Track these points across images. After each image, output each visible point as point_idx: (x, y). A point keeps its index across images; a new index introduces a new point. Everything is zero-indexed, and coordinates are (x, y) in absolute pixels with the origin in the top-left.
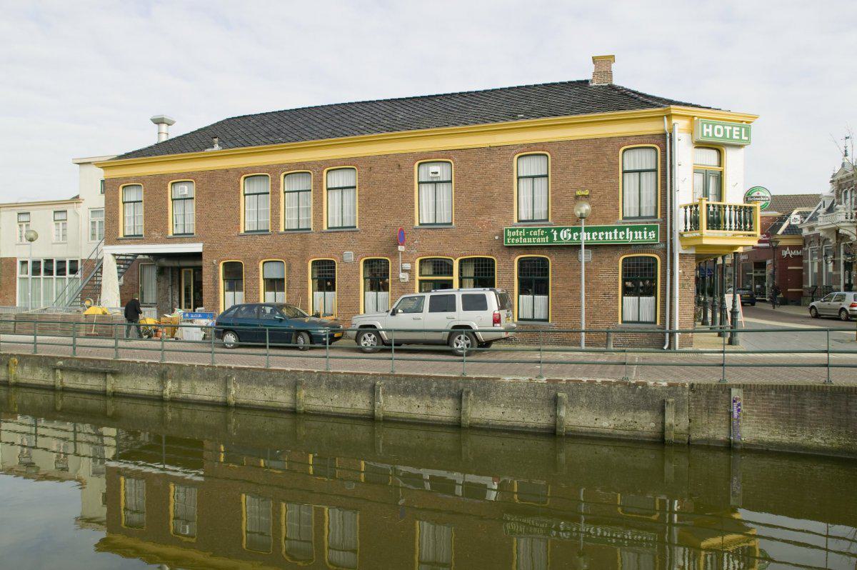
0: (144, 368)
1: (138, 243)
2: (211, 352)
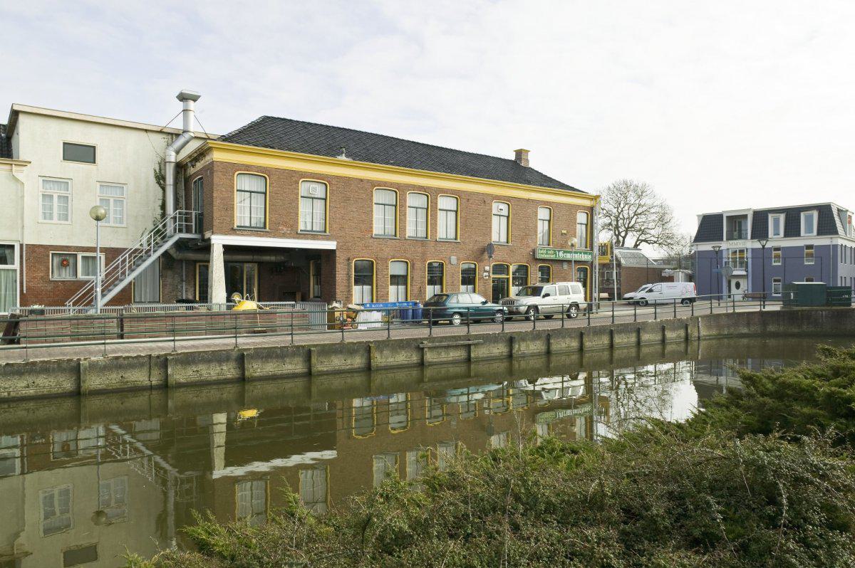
0: (495, 337)
1: (261, 236)
2: (173, 340)
